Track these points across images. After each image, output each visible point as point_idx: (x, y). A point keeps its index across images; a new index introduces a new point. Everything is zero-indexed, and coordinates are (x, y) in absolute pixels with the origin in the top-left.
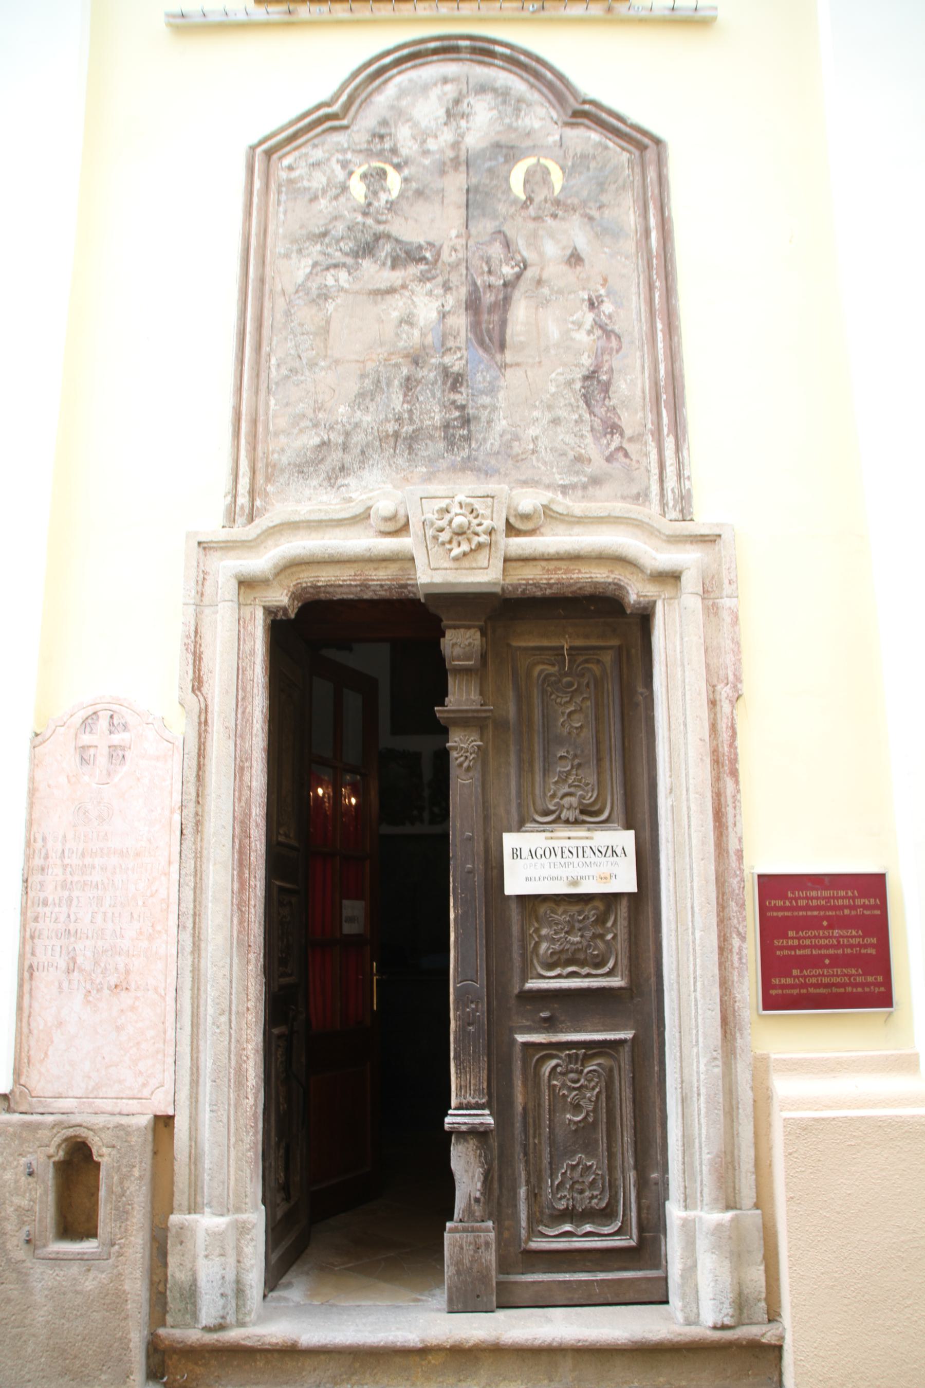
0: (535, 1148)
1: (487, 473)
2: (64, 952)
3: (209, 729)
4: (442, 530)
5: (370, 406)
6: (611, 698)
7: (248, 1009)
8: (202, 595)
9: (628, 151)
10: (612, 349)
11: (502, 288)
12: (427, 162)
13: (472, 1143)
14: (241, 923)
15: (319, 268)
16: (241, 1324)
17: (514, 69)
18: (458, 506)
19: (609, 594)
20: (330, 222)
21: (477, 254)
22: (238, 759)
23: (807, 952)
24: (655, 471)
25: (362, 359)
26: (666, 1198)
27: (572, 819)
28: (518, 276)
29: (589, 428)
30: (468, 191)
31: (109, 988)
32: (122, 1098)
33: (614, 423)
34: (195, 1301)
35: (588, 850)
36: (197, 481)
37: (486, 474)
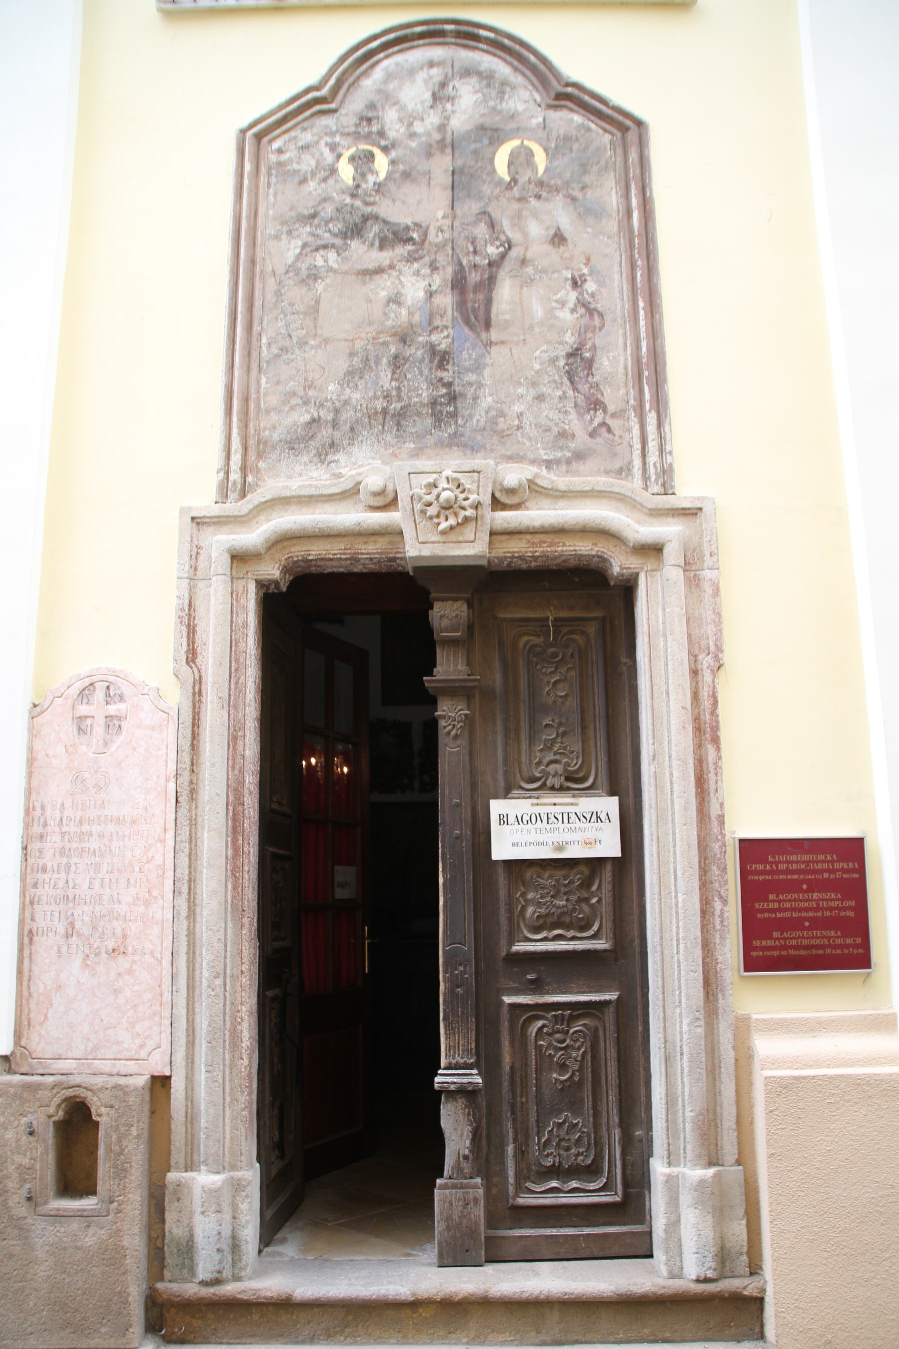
0: (522, 1107)
1: (473, 448)
2: (62, 917)
3: (203, 700)
4: (429, 504)
5: (359, 383)
6: (595, 668)
7: (242, 972)
8: (196, 569)
9: (610, 133)
10: (595, 327)
11: (487, 268)
12: (413, 144)
13: (461, 1102)
14: (235, 888)
15: (308, 249)
16: (237, 1278)
17: (499, 53)
18: (445, 481)
19: (593, 566)
20: (320, 203)
21: (463, 235)
22: (232, 729)
23: (787, 915)
24: (637, 446)
25: (350, 338)
26: (651, 1154)
27: (557, 786)
28: (503, 256)
29: (573, 405)
30: (453, 173)
31: (107, 953)
32: (120, 1059)
33: (597, 399)
34: (192, 1256)
35: (573, 816)
36: (188, 456)
37: (473, 449)
